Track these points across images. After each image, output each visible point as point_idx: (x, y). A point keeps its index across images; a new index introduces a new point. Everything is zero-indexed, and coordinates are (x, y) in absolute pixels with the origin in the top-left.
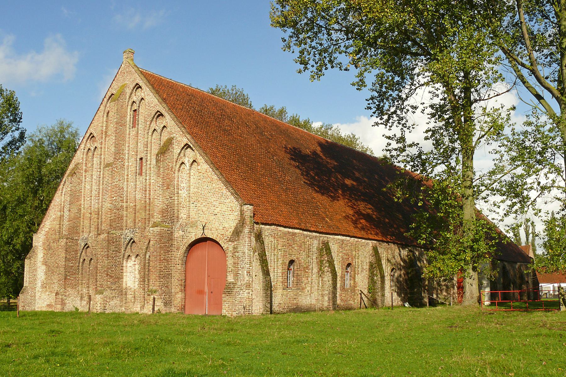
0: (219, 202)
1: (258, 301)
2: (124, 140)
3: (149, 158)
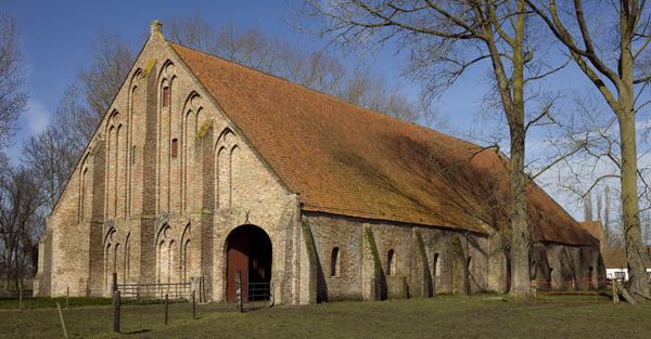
2: (156, 120)
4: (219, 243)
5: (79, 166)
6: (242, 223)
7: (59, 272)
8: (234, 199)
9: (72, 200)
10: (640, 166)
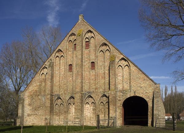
5: (39, 72)
7: (29, 115)
9: (35, 86)
10: (122, 118)
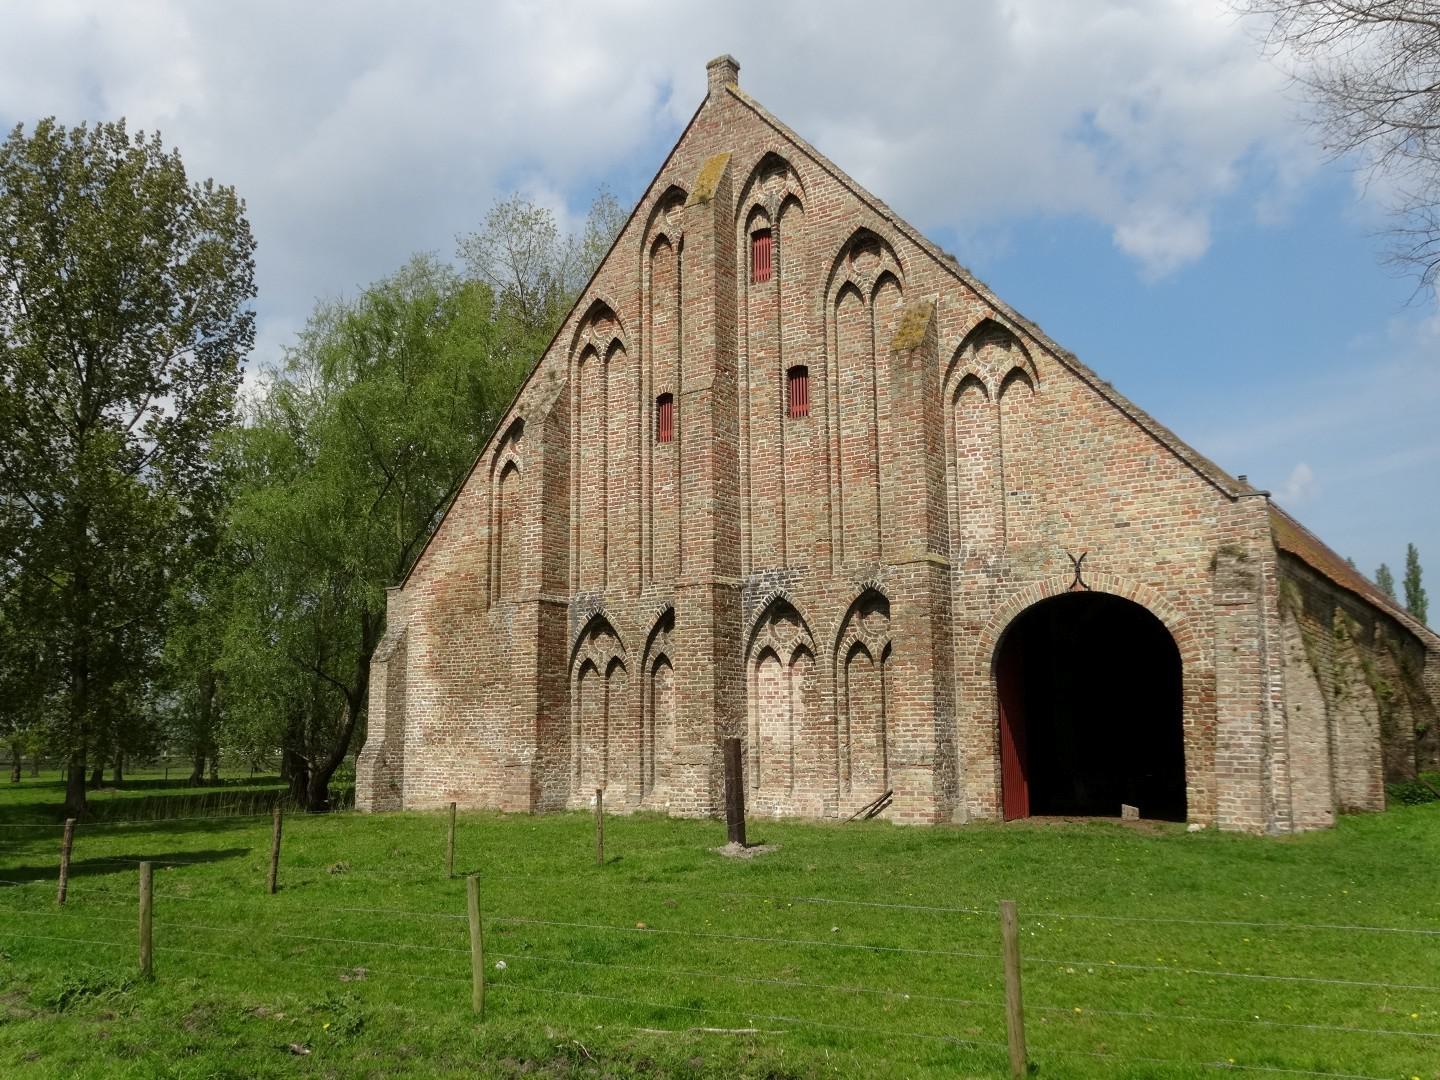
0: (1133, 487)
1: (1312, 788)
2: (734, 316)
3: (831, 365)
4: (974, 654)
6: (1061, 584)
8: (1016, 525)
